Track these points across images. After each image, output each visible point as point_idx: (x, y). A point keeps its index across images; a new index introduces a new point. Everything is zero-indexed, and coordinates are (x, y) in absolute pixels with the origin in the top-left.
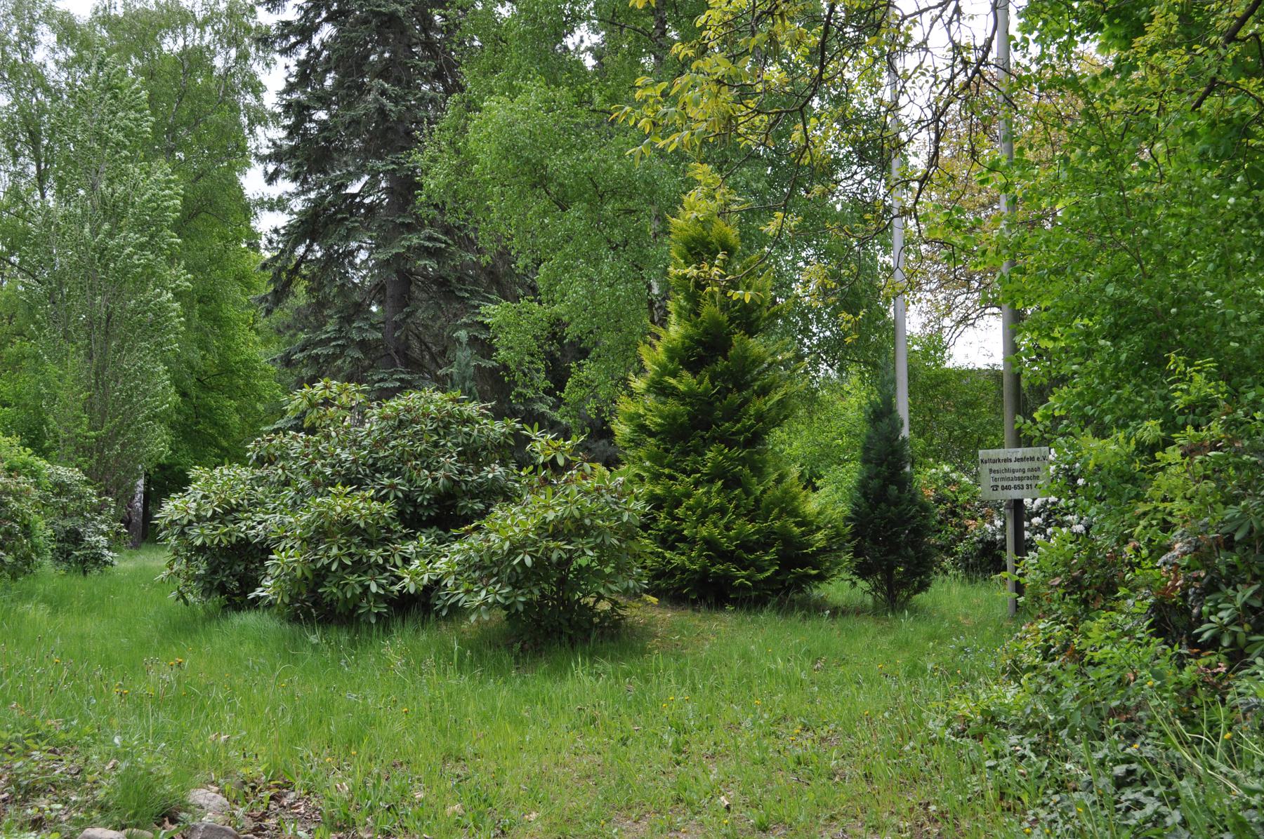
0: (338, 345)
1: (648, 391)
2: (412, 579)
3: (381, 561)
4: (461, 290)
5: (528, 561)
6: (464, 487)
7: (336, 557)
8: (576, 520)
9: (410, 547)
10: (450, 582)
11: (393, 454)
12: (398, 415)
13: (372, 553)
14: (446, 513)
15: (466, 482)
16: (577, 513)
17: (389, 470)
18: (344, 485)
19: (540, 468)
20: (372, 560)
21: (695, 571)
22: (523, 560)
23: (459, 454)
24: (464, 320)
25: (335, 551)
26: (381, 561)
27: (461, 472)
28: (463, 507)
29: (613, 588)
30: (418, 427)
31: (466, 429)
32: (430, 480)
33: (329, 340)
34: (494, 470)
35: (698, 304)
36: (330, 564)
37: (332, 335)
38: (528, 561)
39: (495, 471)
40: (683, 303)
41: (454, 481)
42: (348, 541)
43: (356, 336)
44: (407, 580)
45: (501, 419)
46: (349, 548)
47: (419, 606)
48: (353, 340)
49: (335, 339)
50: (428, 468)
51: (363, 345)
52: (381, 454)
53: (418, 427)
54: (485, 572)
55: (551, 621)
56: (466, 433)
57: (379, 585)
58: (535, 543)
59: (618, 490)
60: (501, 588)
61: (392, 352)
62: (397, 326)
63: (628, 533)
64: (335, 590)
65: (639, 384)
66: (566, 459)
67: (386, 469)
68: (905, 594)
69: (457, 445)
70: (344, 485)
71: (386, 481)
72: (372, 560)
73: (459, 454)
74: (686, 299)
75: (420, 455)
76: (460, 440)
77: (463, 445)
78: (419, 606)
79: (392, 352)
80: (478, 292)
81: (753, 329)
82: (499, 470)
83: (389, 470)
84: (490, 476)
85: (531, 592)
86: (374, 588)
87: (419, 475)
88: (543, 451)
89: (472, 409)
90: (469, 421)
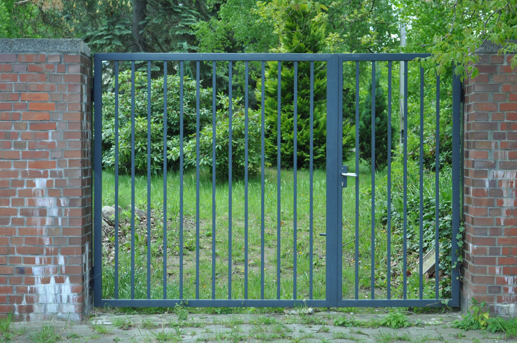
0: (108, 39)
1: (270, 76)
2: (174, 153)
3: (158, 148)
4: (176, 8)
5: (220, 147)
6: (191, 118)
7: (140, 146)
8: (239, 131)
9: (169, 143)
10: (189, 155)
11: (160, 104)
12: (161, 86)
13: (154, 145)
14: (185, 129)
15: (192, 116)
16: (239, 129)
17: (159, 110)
18: (141, 117)
19: (224, 110)
20: (155, 148)
21: (288, 155)
22: (218, 147)
23: (189, 103)
24: (180, 25)
25: (139, 144)
26: (158, 148)
27: (190, 112)
28: (190, 127)
29: (254, 158)
30: (171, 92)
31: (191, 93)
32: (176, 115)
33: (102, 36)
34: (204, 111)
35: (292, 38)
36: (138, 149)
37: (104, 33)
38: (220, 147)
39: (205, 111)
40: (285, 38)
41: (187, 115)
42: (144, 140)
43: (117, 33)
44: (171, 155)
45: (206, 88)
46: (145, 143)
47: (174, 166)
48: (116, 35)
49: (106, 35)
50: (175, 109)
51: (121, 38)
52: (155, 104)
53: (171, 92)
54: (203, 152)
55: (229, 169)
56: (191, 95)
57: (158, 159)
58: (223, 140)
59: (257, 120)
60: (209, 158)
61: (137, 42)
62: (140, 28)
63: (258, 136)
64: (140, 160)
65: (267, 73)
66: (235, 107)
67: (156, 110)
68: (382, 166)
69: (188, 100)
70: (141, 117)
71: (158, 115)
72: (155, 148)
73: (189, 103)
74: (287, 36)
75: (172, 104)
76: (189, 97)
77: (190, 99)
78: (174, 166)
79: (137, 42)
80: (186, 9)
81: (317, 49)
82: (206, 111)
83: (159, 110)
84: (202, 113)
85: (221, 160)
86: (156, 159)
87: (172, 113)
88: (225, 103)
89: (193, 83)
90: (191, 89)
